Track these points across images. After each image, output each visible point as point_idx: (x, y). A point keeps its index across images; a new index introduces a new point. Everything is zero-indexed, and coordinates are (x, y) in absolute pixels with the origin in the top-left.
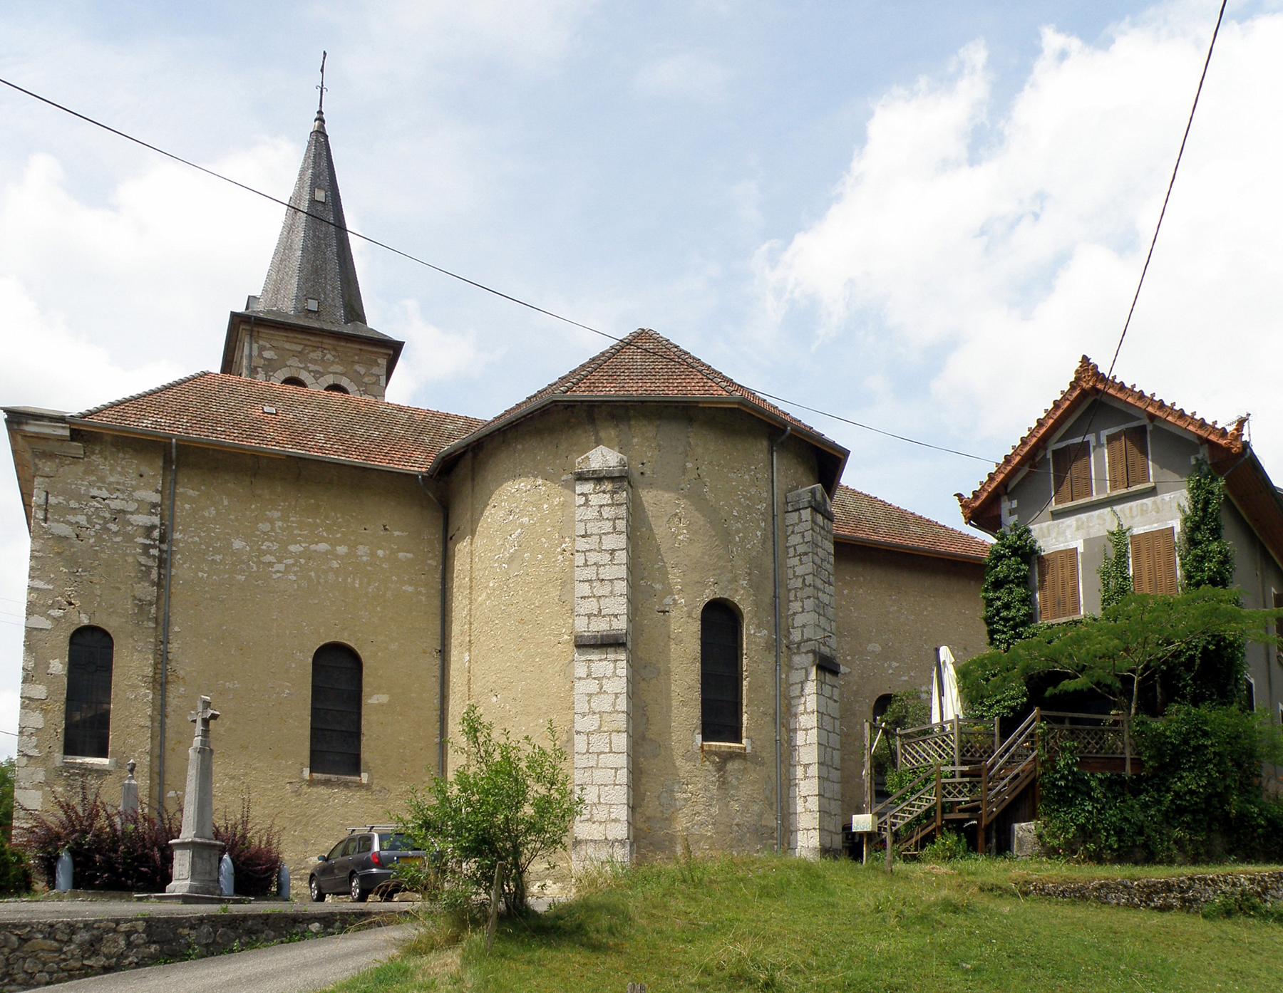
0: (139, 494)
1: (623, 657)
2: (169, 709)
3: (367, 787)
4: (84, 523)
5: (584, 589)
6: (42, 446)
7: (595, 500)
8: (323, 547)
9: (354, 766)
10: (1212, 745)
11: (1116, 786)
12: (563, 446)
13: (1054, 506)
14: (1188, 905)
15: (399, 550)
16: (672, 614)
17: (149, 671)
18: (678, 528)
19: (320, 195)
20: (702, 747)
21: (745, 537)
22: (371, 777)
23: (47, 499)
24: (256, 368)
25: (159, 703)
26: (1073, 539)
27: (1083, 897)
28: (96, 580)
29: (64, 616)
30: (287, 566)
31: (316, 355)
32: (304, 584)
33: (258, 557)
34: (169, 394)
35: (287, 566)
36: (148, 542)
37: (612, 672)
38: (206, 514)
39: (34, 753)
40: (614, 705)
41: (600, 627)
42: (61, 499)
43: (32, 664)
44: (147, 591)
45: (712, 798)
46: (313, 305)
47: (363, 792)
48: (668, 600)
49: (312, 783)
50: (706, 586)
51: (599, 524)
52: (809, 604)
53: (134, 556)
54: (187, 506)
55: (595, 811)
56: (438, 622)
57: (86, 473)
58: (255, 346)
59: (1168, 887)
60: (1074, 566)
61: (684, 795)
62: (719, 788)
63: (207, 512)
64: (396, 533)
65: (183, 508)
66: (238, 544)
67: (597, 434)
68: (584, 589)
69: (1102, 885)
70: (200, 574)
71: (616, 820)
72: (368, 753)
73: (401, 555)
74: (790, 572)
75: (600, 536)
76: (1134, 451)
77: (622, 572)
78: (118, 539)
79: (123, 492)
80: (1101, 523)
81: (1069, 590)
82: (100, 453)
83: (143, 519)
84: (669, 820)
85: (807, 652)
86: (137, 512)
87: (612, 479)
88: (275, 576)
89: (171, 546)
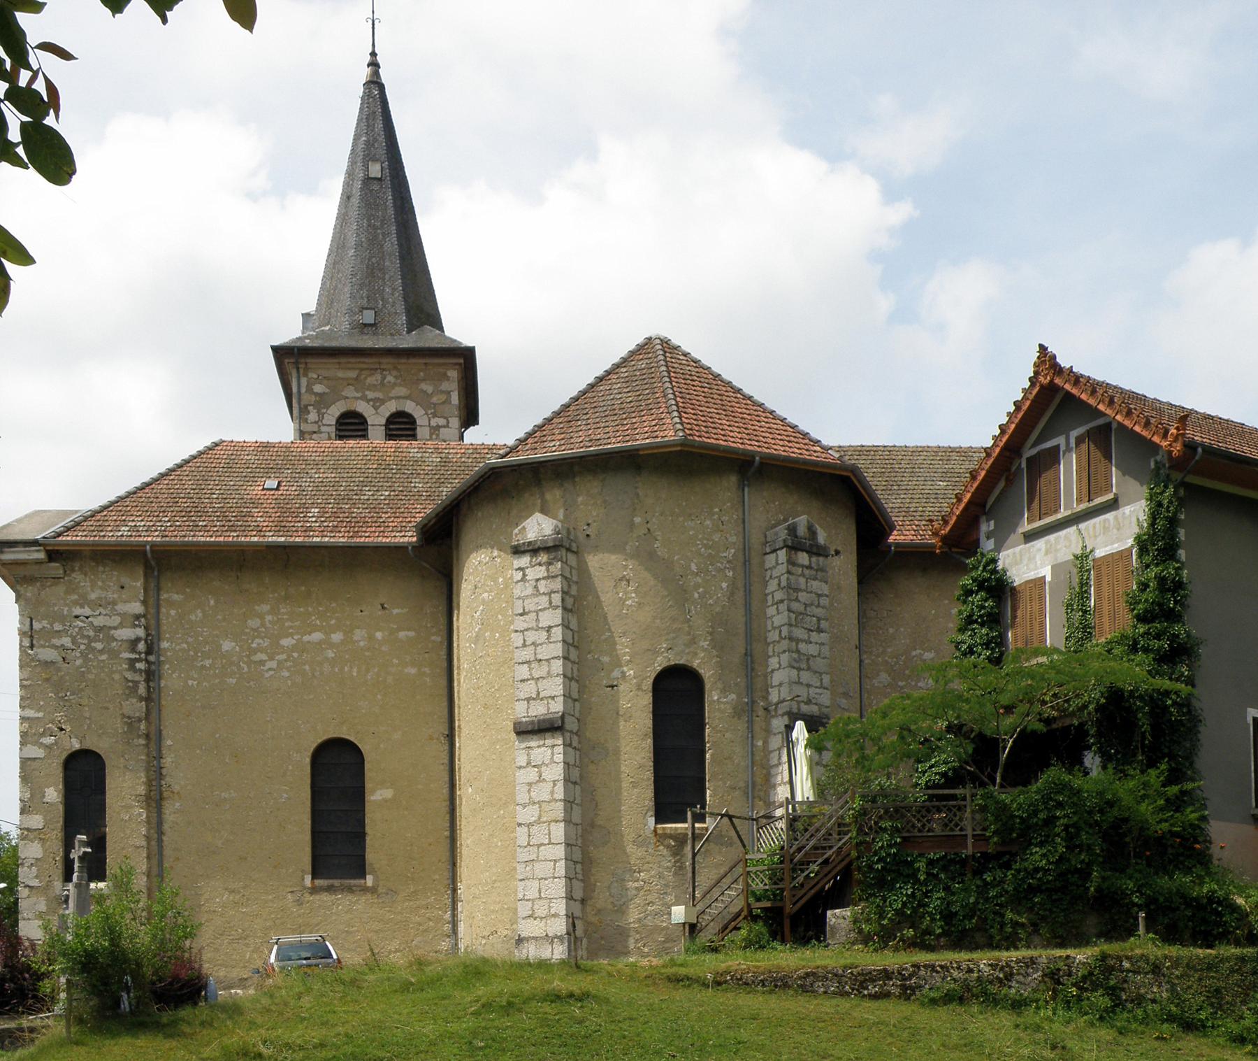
0: (121, 607)
1: (560, 741)
2: (166, 827)
3: (373, 890)
4: (70, 645)
5: (523, 671)
6: (21, 571)
7: (532, 574)
8: (317, 636)
9: (358, 867)
10: (1065, 816)
11: (955, 866)
12: (514, 512)
13: (1026, 526)
14: (907, 993)
15: (399, 629)
16: (621, 688)
17: (142, 790)
18: (626, 593)
19: (375, 170)
20: (655, 831)
21: (705, 592)
22: (376, 879)
23: (31, 625)
24: (306, 406)
25: (154, 821)
26: (1043, 565)
27: (786, 986)
28: (85, 701)
29: (56, 743)
30: (279, 662)
31: (375, 379)
32: (299, 679)
33: (248, 656)
34: (162, 485)
35: (279, 662)
36: (133, 656)
37: (550, 756)
38: (193, 618)
39: (35, 883)
40: (552, 793)
41: (539, 710)
42: (45, 623)
43: (28, 795)
44: (136, 707)
45: (667, 886)
46: (369, 317)
47: (369, 896)
48: (616, 673)
49: (314, 890)
50: (656, 652)
51: (536, 600)
52: (785, 658)
53: (120, 672)
54: (173, 612)
55: (536, 907)
56: (445, 704)
57: (67, 592)
58: (304, 381)
59: (887, 975)
60: (1042, 598)
61: (636, 884)
62: (675, 874)
63: (192, 613)
64: (395, 611)
65: (169, 614)
66: (227, 645)
67: (542, 496)
68: (523, 671)
69: (808, 975)
70: (190, 682)
71: (555, 915)
72: (372, 856)
73: (402, 634)
74: (769, 623)
75: (537, 612)
76: (1097, 454)
77: (558, 649)
78: (104, 657)
79: (105, 608)
80: (1065, 544)
81: (1036, 627)
82: (81, 569)
83: (127, 633)
84: (621, 910)
85: (783, 715)
86: (121, 626)
87: (547, 549)
88: (267, 675)
89: (159, 656)
